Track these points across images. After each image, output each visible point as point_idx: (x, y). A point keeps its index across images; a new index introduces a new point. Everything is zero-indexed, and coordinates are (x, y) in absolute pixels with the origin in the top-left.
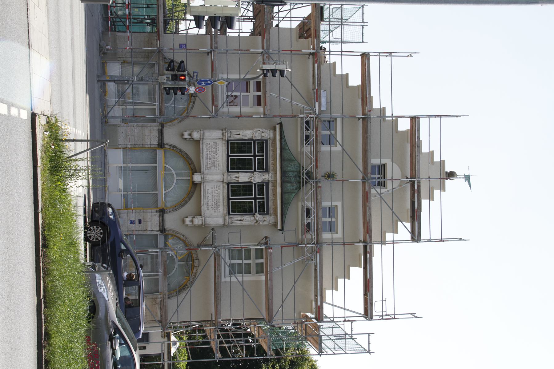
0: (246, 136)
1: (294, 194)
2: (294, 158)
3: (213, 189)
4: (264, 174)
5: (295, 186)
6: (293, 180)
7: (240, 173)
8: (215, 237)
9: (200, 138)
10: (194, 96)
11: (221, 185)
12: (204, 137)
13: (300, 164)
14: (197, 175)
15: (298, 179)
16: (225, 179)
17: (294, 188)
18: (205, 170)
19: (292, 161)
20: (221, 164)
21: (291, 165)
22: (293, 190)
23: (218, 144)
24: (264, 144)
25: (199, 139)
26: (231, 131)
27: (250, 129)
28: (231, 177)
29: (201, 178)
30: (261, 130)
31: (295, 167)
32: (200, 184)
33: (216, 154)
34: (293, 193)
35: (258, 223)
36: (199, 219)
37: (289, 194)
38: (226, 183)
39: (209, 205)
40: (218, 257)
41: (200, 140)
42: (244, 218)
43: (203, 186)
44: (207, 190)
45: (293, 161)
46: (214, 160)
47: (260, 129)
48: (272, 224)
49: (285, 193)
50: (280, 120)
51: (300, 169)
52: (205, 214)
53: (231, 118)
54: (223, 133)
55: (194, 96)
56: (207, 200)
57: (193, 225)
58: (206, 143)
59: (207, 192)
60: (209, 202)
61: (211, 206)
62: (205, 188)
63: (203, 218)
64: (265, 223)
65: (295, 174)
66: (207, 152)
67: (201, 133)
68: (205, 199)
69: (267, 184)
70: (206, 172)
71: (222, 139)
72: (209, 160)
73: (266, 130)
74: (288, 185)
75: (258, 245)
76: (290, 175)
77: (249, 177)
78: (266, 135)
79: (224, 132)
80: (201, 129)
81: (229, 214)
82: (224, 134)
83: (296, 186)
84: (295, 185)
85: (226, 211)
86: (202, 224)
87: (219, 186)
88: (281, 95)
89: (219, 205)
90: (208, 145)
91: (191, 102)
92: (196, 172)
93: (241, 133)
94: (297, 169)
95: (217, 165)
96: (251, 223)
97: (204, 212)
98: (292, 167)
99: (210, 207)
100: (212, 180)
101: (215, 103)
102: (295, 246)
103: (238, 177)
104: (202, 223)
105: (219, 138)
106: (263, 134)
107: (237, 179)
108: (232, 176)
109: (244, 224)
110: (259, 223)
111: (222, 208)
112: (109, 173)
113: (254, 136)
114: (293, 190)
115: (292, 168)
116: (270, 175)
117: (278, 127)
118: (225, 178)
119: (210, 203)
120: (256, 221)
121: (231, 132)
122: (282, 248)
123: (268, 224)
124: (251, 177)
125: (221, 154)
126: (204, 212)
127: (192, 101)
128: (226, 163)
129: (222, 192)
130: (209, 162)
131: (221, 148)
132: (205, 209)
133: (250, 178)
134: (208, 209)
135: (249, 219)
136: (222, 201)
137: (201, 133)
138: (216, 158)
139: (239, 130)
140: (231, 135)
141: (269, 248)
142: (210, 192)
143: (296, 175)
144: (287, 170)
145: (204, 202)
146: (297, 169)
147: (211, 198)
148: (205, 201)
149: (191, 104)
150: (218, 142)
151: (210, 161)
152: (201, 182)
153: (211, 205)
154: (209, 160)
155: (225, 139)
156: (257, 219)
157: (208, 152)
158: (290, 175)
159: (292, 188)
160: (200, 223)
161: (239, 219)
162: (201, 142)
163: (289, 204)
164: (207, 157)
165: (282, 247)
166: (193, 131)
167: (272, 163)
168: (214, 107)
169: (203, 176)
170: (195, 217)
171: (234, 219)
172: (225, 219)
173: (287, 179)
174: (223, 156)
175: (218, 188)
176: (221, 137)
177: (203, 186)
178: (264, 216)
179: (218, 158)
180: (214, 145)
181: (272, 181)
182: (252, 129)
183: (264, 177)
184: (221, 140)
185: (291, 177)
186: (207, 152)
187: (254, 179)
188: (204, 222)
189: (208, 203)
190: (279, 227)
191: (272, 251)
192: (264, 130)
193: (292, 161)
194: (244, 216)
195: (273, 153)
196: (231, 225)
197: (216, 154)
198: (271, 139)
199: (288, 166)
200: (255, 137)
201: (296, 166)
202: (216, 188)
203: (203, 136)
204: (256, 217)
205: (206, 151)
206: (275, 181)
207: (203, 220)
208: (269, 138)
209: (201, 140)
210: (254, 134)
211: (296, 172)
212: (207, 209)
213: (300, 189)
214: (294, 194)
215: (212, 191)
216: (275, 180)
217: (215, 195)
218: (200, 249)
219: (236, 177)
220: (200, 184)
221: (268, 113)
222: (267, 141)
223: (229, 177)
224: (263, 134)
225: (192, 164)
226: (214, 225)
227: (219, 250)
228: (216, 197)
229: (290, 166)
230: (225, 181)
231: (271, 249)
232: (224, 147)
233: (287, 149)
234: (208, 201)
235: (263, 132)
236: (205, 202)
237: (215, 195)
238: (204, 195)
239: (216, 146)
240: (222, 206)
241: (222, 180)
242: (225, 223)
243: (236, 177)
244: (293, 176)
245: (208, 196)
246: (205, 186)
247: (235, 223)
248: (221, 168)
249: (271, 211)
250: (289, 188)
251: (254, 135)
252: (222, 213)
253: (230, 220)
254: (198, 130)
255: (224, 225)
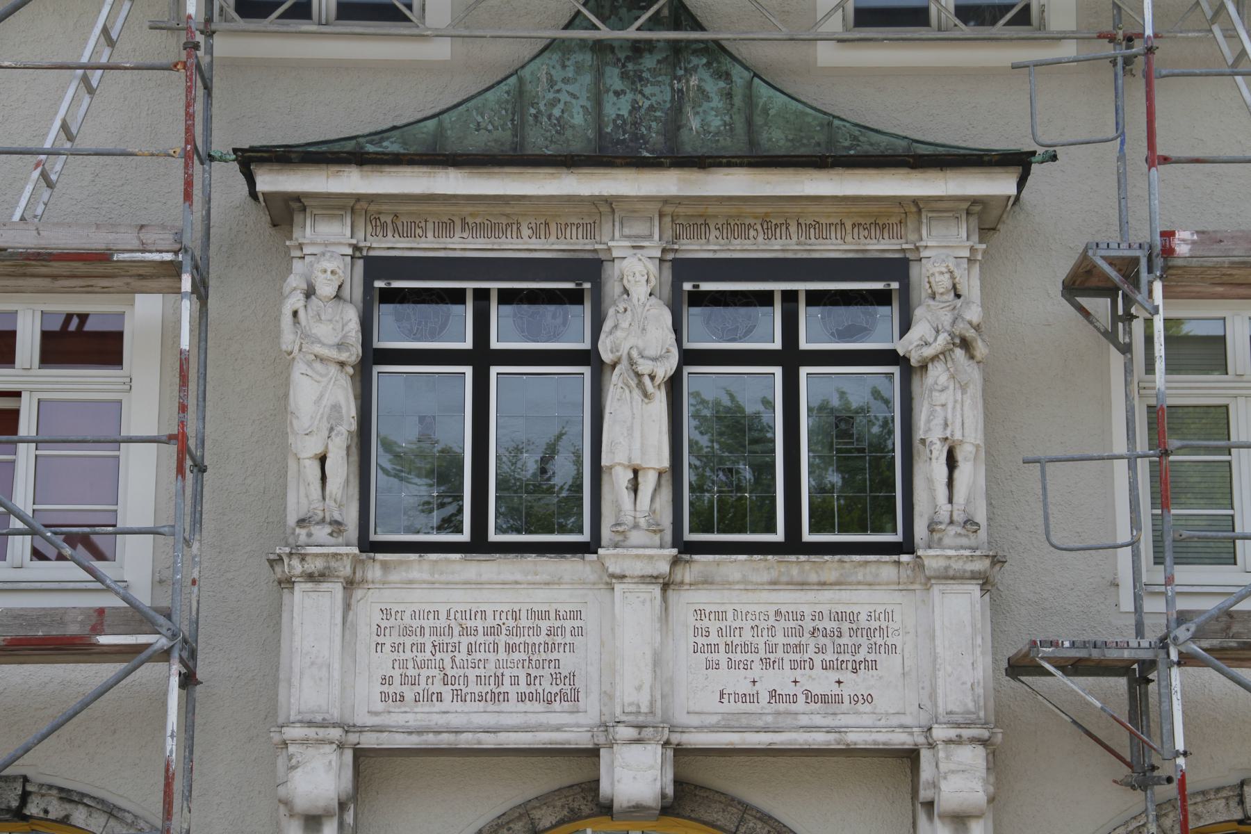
0: (336, 408)
1: (763, 91)
2: (504, 87)
3: (722, 657)
4: (612, 289)
5: (700, 79)
6: (658, 94)
7: (605, 462)
8: (1084, 645)
9: (341, 746)
10: (25, 797)
11: (686, 602)
12: (335, 715)
13: (551, 45)
14: (618, 770)
15: (649, 62)
16: (650, 570)
17: (713, 87)
18: (581, 719)
19: (520, 100)
20: (541, 598)
21: (553, 103)
22: (729, 95)
23: (386, 613)
24: (397, 284)
25: (349, 755)
26: (292, 520)
27: (287, 383)
28: (636, 526)
29: (638, 741)
30: (295, 301)
31: (566, 81)
32: (681, 754)
33: (465, 631)
34: (750, 99)
35: (970, 333)
36: (943, 767)
37: (759, 120)
38: (675, 562)
39: (836, 690)
40: (1236, 628)
41: (360, 754)
42: (935, 436)
43: (700, 729)
44: (729, 707)
45: (521, 90)
46: (510, 648)
47: (287, 319)
48: (975, 238)
49: (752, 143)
50: (222, 159)
51: (583, 44)
52: (907, 720)
53: (197, 521)
54: (310, 577)
55: (25, 797)
56: (801, 705)
57: (990, 816)
58: (380, 706)
59: (741, 707)
60: (817, 690)
61: (847, 676)
62: (713, 720)
63: (939, 733)
64: (972, 285)
65: (613, 78)
66: (447, 696)
67: (305, 742)
68: (789, 721)
69: (683, 269)
70: (591, 710)
71: (350, 584)
72: (506, 687)
73: (298, 266)
74: (695, 123)
75: (1126, 349)
76: (625, 113)
77: (637, 394)
78: (330, 266)
79: (297, 567)
80: (276, 738)
81: (906, 547)
82: (315, 566)
83: (705, 74)
84: (694, 81)
85: (883, 567)
86: (984, 742)
87: (700, 613)
88: (32, 145)
89: (839, 617)
90: (396, 688)
91: (65, 821)
92: (597, 781)
93: (309, 448)
94: (579, 68)
95: (544, 625)
96: (975, 389)
97: (892, 729)
98: (564, 97)
99: (855, 684)
100: (657, 662)
101: (73, 629)
102: (1148, 63)
103: (636, 472)
104: (974, 740)
105: (347, 607)
106: (326, 289)
107: (648, 482)
108: (629, 520)
109: (980, 440)
110: (977, 328)
111: (863, 595)
112: (526, 723)
113: (334, 354)
114: (729, 95)
115: (574, 96)
116: (619, 247)
117: (270, 181)
118: (640, 568)
119: (823, 683)
120: (959, 353)
121: (302, 522)
122: (1166, 160)
123: (976, 269)
124: (639, 375)
125: (460, 599)
126: (892, 729)
127: (56, 810)
128: (532, 558)
129: (746, 597)
130: (523, 688)
131: (418, 599)
132: (867, 720)
133: (640, 384)
134: (868, 699)
135: (940, 398)
136: (810, 596)
137: (305, 742)
138: (493, 631)
139: (292, 464)
140: (323, 521)
141: (1168, 252)
142: (738, 682)
143: (624, 76)
144: (590, 134)
145: (817, 728)
146: (579, 68)
147: (789, 674)
148: (804, 720)
149: (79, 817)
150: (377, 617)
151: (515, 681)
152: (666, 744)
153: (834, 676)
154: (506, 687)
155: (356, 562)
156: (943, 339)
157: (447, 691)
158: (625, 113)
159: (716, 102)
160: (974, 757)
161: (940, 470)
162: (369, 741)
163: (829, 121)
164: (481, 698)
165: (1155, 160)
166: (286, 803)
167: (536, 233)
168: (103, 640)
169: (624, 732)
170: (924, 794)
171: (944, 508)
172: (946, 576)
173: (654, 134)
174: (479, 584)
175: (714, 626)
176: (338, 589)
177: (700, 729)
178: (920, 289)
179: (490, 622)
180: (395, 648)
181: (668, 234)
182: (282, 365)
183: (640, 291)
184: (358, 593)
185: (635, 108)
186: (447, 696)
187: (654, 359)
188: (968, 725)
189: (824, 699)
190: (1001, 185)
191: (1182, 235)
192: (295, 281)
193: (520, 100)
194: (919, 434)
195: (464, 225)
196: (983, 534)
197: (465, 631)
198: (360, 235)
199: (561, 125)
200: (340, 346)
201: (558, 74)
202: (714, 639)
203: (324, 725)
204: (928, 352)
205: (438, 706)
206: (666, 207)
207: (952, 733)
208: (356, 248)
209: (353, 738)
210: (318, 349)
211: (599, 75)
212: (867, 708)
213: (716, 42)
214: (763, 91)
215: (732, 665)
216: (661, 215)
217: (760, 641)
218: (1181, 761)
219: (635, 487)
220: (681, 754)
221: (166, 239)
222: (375, 267)
223: (636, 537)
224: (326, 289)
225: (536, 814)
226: (989, 659)
227: (1183, 618)
228: (780, 639)
229: (556, 112)
230: (664, 568)
231: (1168, 235)
232: (415, 574)
233: (440, 124)
234: (808, 694)
235: (310, 293)
236: (818, 720)
237: (760, 641)
238: (766, 730)
239: (407, 631)
240: (845, 595)
241: (657, 590)
242: (974, 576)
243: (635, 487)
244: (629, 96)
245: (773, 694)
246: (695, 721)
247: (968, 502)
248: (564, 599)
249: (881, 246)
250: (716, 123)
251: (325, 352)
252: (898, 597)
253: (947, 541)
254: (281, 762)
255: (986, 583)
